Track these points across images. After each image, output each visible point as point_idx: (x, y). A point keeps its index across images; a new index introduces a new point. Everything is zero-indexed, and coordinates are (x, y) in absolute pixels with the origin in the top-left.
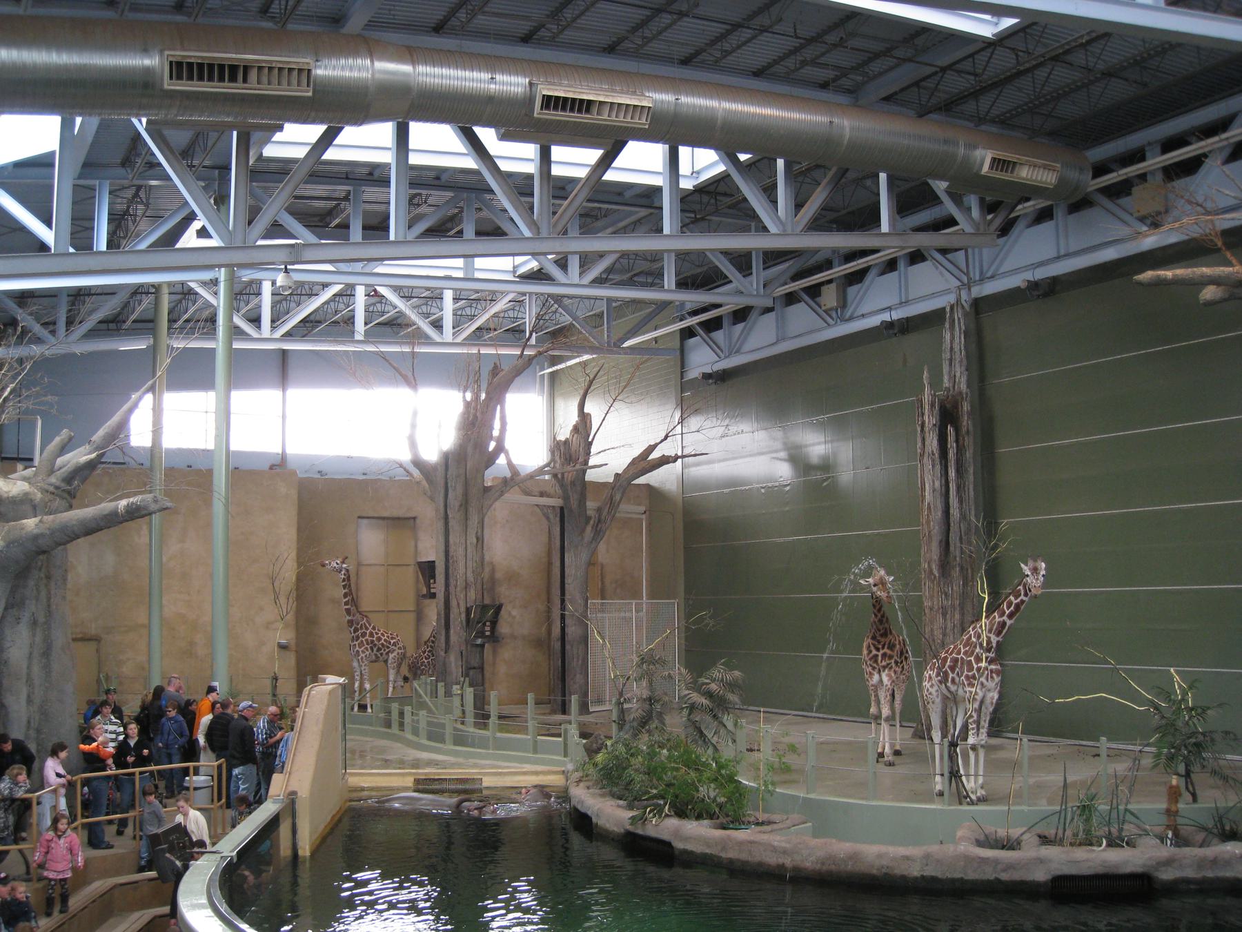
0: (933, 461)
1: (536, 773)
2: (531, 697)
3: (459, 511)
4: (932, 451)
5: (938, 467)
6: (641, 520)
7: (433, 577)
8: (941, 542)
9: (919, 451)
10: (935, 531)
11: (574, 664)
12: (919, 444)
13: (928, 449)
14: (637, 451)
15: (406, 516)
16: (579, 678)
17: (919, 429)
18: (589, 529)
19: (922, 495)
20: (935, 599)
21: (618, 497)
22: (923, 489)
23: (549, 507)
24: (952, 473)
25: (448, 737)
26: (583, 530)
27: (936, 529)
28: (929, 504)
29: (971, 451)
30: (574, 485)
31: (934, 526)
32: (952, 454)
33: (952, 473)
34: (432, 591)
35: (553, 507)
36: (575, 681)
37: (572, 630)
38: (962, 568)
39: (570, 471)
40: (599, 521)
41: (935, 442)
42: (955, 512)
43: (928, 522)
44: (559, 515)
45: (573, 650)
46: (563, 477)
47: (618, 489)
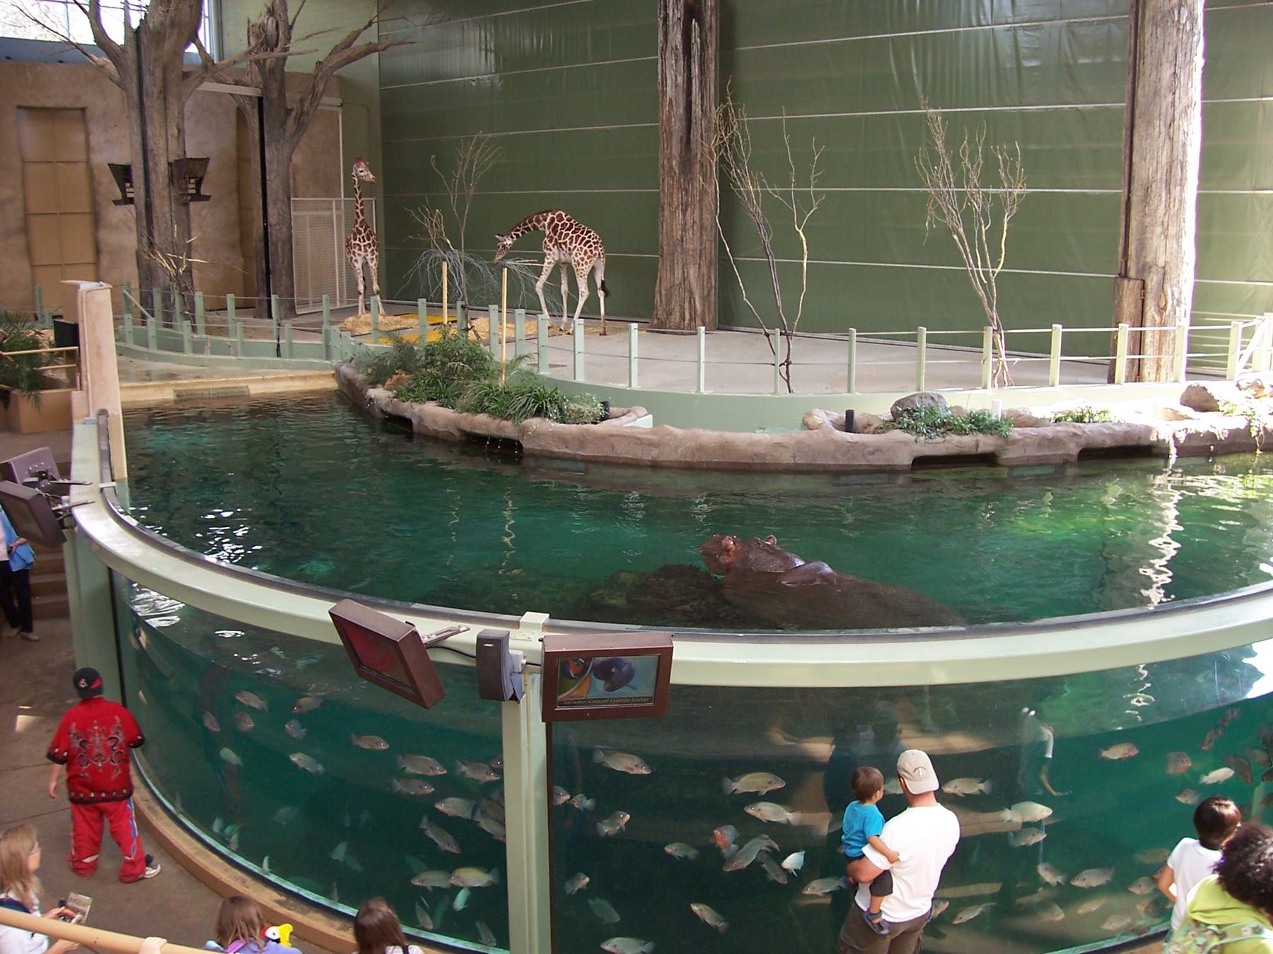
0: (676, 55)
1: (304, 378)
2: (230, 299)
4: (676, 46)
5: (681, 62)
6: (338, 113)
7: (129, 180)
8: (682, 137)
9: (660, 45)
10: (676, 127)
11: (278, 263)
12: (661, 38)
13: (671, 44)
14: (339, 38)
15: (73, 106)
16: (285, 279)
17: (661, 22)
18: (291, 121)
19: (663, 91)
20: (675, 196)
21: (321, 87)
22: (664, 84)
23: (246, 96)
24: (695, 70)
25: (187, 346)
26: (284, 123)
27: (677, 125)
28: (670, 99)
29: (714, 47)
30: (274, 73)
31: (675, 122)
32: (695, 50)
33: (695, 70)
34: (129, 195)
35: (250, 97)
36: (278, 279)
37: (276, 233)
38: (702, 165)
39: (271, 57)
40: (302, 114)
41: (679, 36)
42: (697, 109)
43: (669, 119)
44: (257, 106)
45: (277, 250)
46: (265, 64)
47: (321, 79)
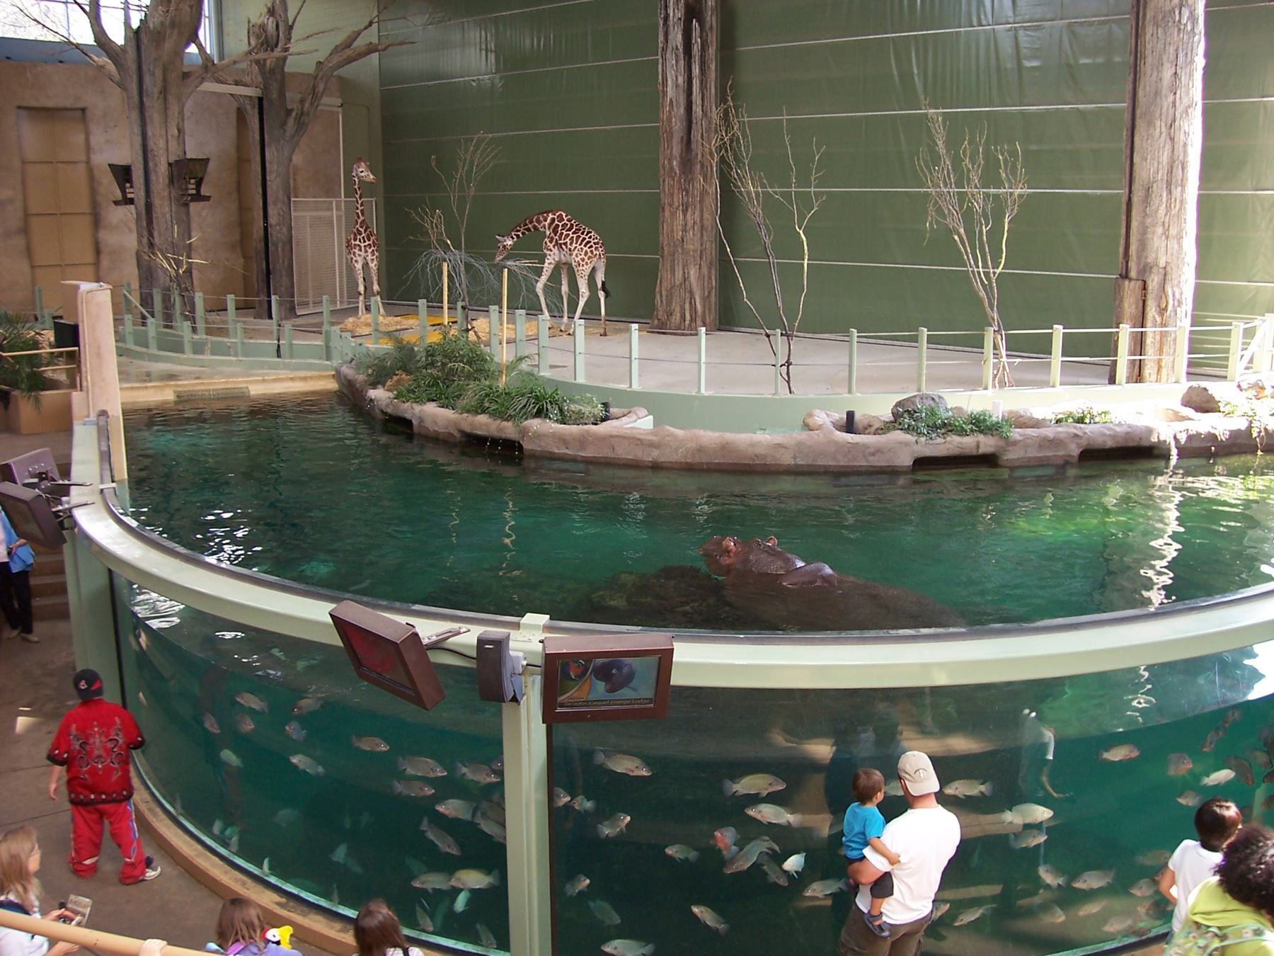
0: (677, 56)
1: (305, 379)
2: (231, 300)
3: (158, 98)
4: (677, 46)
5: (682, 62)
6: (338, 113)
7: (129, 180)
8: (682, 138)
9: (661, 45)
10: (677, 127)
11: (278, 264)
12: (661, 38)
13: (671, 44)
14: (340, 38)
15: (73, 107)
16: (285, 280)
17: (661, 23)
18: (291, 122)
19: (663, 91)
20: (675, 196)
21: (321, 87)
22: (665, 84)
23: (246, 97)
24: (696, 71)
25: (187, 347)
26: (284, 124)
27: (678, 126)
28: (671, 100)
29: (714, 47)
30: (274, 73)
31: (675, 122)
32: (696, 50)
33: (696, 71)
34: (129, 196)
35: (251, 97)
36: (279, 280)
37: (276, 234)
38: (702, 166)
39: (271, 57)
40: (302, 114)
41: (680, 37)
42: (697, 110)
43: (670, 119)
44: (257, 106)
45: (277, 250)
46: (265, 64)
47: (321, 79)
